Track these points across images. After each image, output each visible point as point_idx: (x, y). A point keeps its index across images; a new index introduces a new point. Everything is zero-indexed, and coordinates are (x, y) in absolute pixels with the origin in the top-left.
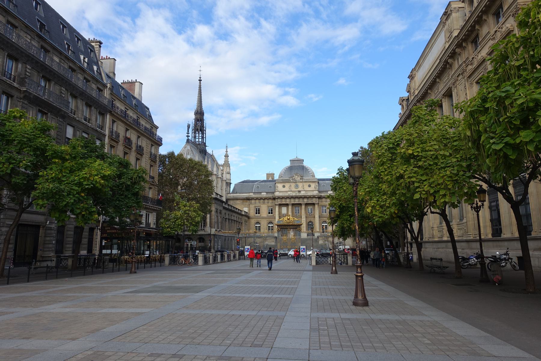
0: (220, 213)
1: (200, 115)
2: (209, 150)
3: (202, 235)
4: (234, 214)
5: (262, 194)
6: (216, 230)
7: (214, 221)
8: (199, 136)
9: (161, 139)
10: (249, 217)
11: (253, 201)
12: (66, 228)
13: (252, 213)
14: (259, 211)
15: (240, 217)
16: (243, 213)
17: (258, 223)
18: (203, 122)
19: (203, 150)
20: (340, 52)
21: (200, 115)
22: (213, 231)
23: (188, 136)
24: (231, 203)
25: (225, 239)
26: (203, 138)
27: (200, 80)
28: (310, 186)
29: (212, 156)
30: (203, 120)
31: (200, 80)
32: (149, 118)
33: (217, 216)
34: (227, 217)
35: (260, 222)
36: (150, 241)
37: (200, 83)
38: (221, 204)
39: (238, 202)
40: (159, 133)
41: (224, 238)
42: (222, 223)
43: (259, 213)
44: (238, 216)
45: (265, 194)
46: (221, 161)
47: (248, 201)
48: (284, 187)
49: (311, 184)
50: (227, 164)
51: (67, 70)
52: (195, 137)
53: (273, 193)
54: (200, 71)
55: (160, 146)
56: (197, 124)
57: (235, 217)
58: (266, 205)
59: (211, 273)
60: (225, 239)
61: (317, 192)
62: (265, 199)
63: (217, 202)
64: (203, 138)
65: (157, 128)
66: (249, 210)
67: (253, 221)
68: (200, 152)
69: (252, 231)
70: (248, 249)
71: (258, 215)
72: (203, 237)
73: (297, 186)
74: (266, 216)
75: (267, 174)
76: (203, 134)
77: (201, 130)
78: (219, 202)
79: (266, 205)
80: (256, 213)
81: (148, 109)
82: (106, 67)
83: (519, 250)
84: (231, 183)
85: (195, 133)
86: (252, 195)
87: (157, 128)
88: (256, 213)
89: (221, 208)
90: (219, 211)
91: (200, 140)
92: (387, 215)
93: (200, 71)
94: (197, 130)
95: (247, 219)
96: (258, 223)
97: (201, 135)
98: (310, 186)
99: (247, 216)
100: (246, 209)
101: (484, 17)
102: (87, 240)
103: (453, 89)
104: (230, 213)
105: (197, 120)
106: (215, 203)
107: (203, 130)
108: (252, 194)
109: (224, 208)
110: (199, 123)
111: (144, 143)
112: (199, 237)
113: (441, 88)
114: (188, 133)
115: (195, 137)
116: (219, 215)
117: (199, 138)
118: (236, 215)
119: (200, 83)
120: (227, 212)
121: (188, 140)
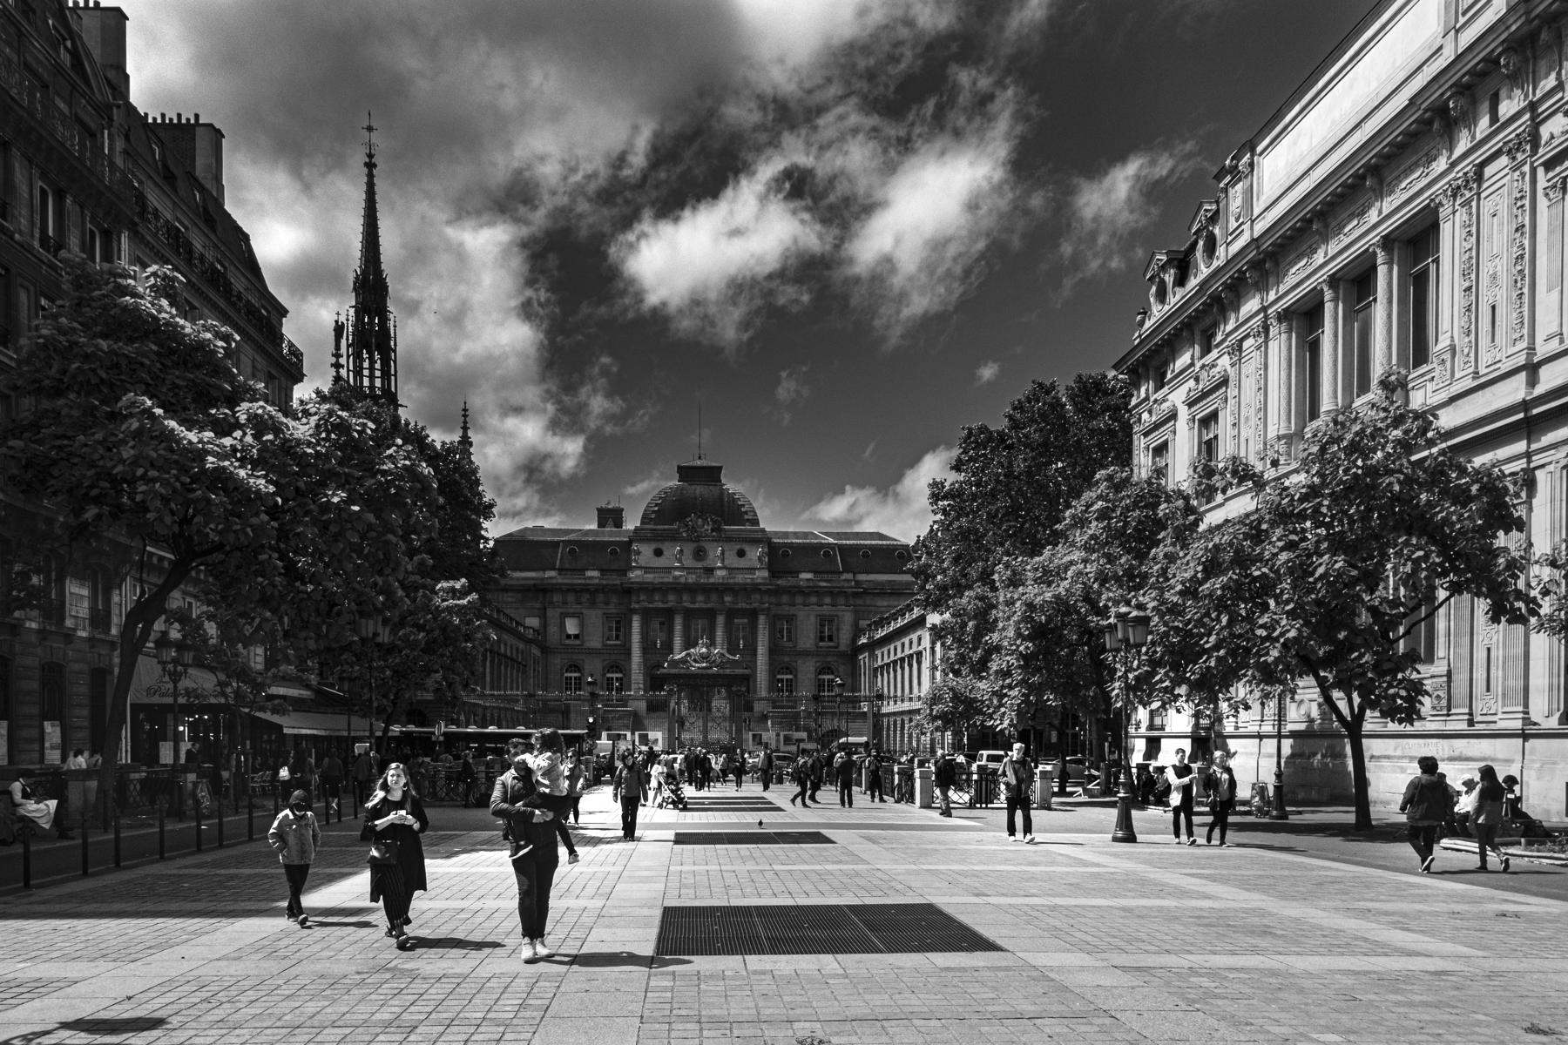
5: (589, 573)
8: (372, 369)
11: (557, 598)
23: (337, 366)
26: (386, 374)
28: (741, 554)
45: (595, 574)
48: (658, 553)
49: (747, 548)
52: (358, 372)
53: (623, 572)
54: (370, 129)
58: (600, 612)
59: (1192, 875)
61: (766, 574)
62: (596, 591)
64: (386, 374)
73: (699, 554)
74: (599, 645)
79: (600, 612)
83: (1372, 757)
93: (370, 129)
98: (741, 554)
101: (849, 138)
102: (85, 712)
103: (1444, 212)
108: (553, 573)
113: (1386, 212)
114: (337, 355)
115: (358, 372)
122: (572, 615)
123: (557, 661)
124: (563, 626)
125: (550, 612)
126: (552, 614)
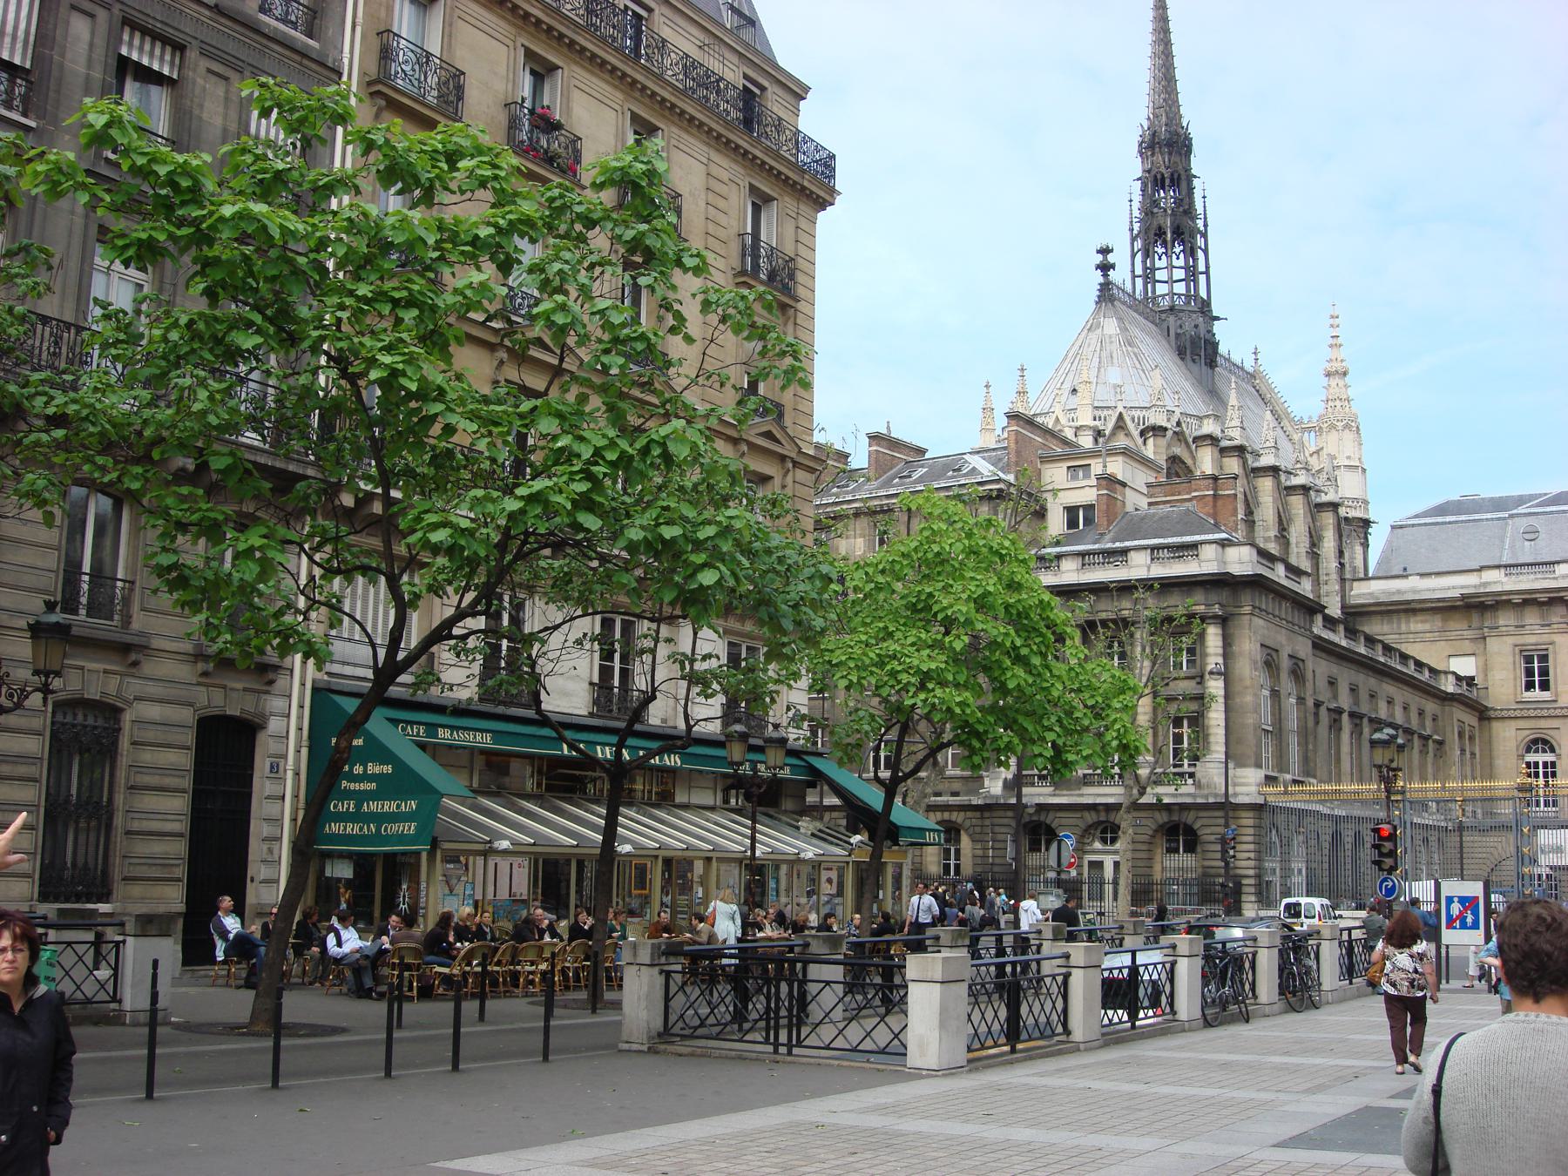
0: (1297, 674)
1: (1168, 155)
2: (1231, 340)
3: (1184, 807)
4: (1389, 688)
6: (1270, 780)
7: (1250, 720)
10: (1484, 714)
11: (1505, 619)
12: (127, 717)
13: (1503, 683)
14: (1544, 672)
15: (1431, 706)
16: (1449, 686)
17: (1541, 743)
18: (1191, 190)
19: (1194, 341)
21: (1168, 155)
22: (1248, 785)
24: (1375, 628)
25: (1336, 838)
29: (1252, 380)
30: (1190, 177)
33: (1275, 694)
34: (1345, 701)
35: (1557, 738)
38: (1297, 617)
39: (1417, 625)
40: (815, 122)
41: (1327, 830)
42: (1305, 734)
43: (1545, 686)
44: (1416, 700)
46: (1304, 402)
47: (1475, 617)
52: (1149, 276)
55: (822, 204)
56: (1155, 203)
57: (1393, 704)
60: (1336, 838)
63: (1265, 602)
64: (1192, 274)
65: (797, 92)
66: (1485, 669)
67: (1507, 737)
68: (1181, 353)
69: (1507, 779)
70: (1469, 903)
71: (1537, 694)
72: (1189, 818)
76: (1191, 252)
77: (1178, 233)
78: (1285, 609)
80: (1530, 686)
84: (1366, 523)
85: (1147, 254)
86: (1497, 581)
88: (1530, 686)
89: (1304, 648)
90: (1285, 664)
92: (1148, 916)
95: (1470, 719)
96: (1541, 743)
99: (1471, 702)
100: (1465, 666)
104: (1367, 682)
105: (1154, 182)
106: (1257, 610)
107: (1194, 232)
109: (1320, 646)
110: (1167, 198)
111: (689, 168)
112: (1162, 818)
115: (1149, 276)
116: (1287, 685)
118: (1400, 694)
120: (1346, 676)
121: (1106, 293)
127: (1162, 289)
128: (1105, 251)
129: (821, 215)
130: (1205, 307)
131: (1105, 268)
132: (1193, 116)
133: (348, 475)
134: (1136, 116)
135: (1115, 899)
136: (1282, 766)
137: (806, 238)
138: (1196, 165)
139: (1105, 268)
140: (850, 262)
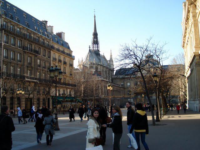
1: (95, 35)
9: (74, 57)
16: (121, 86)
20: (47, 107)
21: (95, 35)
27: (95, 17)
31: (95, 17)
32: (69, 48)
36: (56, 105)
37: (95, 18)
40: (73, 54)
50: (111, 60)
51: (35, 40)
52: (93, 47)
56: (94, 40)
64: (97, 47)
65: (72, 52)
75: (47, 21)
76: (97, 45)
77: (96, 43)
81: (68, 44)
82: (49, 31)
87: (72, 52)
91: (96, 49)
94: (95, 43)
97: (96, 46)
105: (94, 38)
110: (95, 40)
111: (67, 60)
115: (93, 47)
117: (96, 48)
119: (95, 18)
122: (128, 82)
123: (126, 90)
124: (127, 84)
125: (125, 82)
126: (125, 82)
127: (95, 49)
128: (90, 46)
129: (74, 60)
130: (99, 51)
131: (90, 48)
132: (98, 32)
133: (56, 82)
134: (93, 31)
135: (197, 107)
136: (105, 95)
137: (73, 62)
138: (98, 37)
139: (90, 48)
140: (96, 136)
